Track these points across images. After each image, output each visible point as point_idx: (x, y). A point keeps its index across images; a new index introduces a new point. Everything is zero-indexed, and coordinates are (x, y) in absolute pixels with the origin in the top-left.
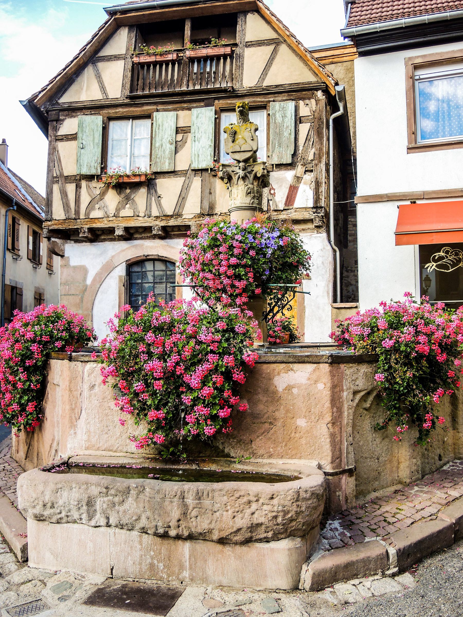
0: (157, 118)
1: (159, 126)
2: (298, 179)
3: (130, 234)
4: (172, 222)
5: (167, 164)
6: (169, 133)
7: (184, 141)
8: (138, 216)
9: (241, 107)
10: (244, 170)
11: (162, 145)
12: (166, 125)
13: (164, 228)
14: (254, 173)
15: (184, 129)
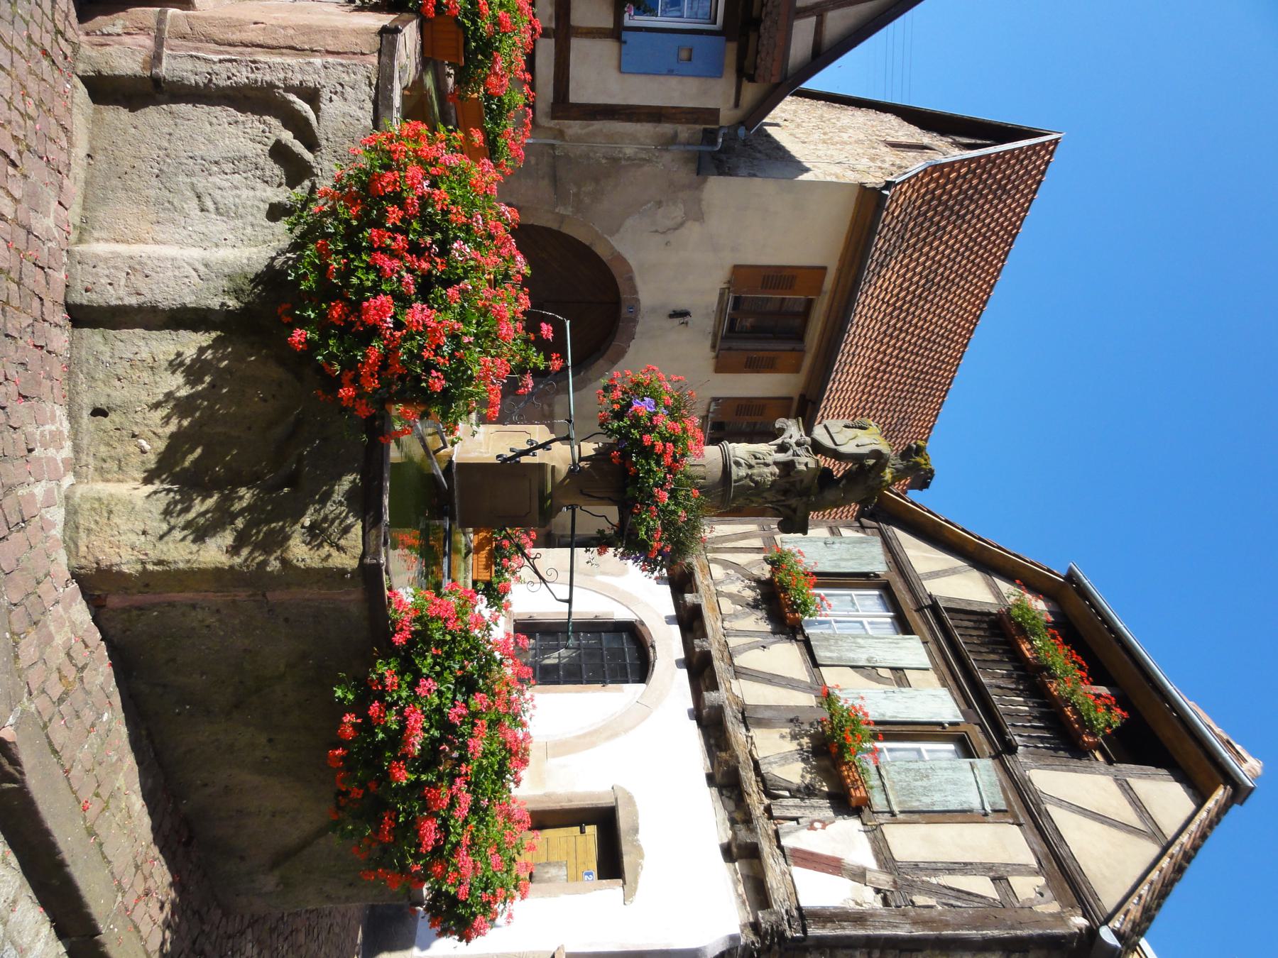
2: (859, 875)
3: (690, 621)
4: (718, 665)
7: (880, 680)
8: (723, 620)
13: (706, 658)
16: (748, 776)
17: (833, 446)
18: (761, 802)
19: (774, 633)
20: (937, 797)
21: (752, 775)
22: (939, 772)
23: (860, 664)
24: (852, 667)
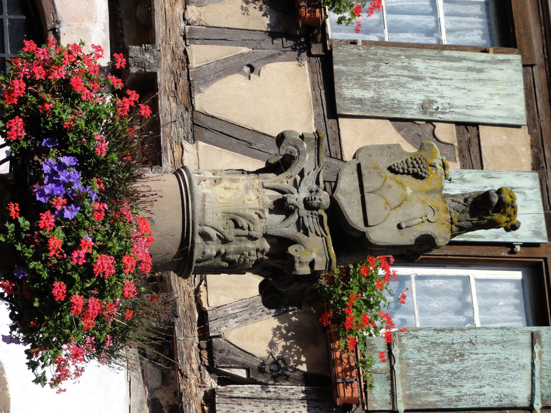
0: (504, 66)
1: (480, 71)
4: (168, 106)
5: (358, 93)
6: (457, 103)
9: (500, 199)
11: (419, 79)
12: (482, 92)
14: (300, 235)
15: (474, 149)
16: (188, 340)
17: (360, 226)
18: (201, 383)
19: (273, 34)
20: (469, 387)
21: (194, 338)
22: (481, 348)
23: (408, 115)
24: (392, 120)
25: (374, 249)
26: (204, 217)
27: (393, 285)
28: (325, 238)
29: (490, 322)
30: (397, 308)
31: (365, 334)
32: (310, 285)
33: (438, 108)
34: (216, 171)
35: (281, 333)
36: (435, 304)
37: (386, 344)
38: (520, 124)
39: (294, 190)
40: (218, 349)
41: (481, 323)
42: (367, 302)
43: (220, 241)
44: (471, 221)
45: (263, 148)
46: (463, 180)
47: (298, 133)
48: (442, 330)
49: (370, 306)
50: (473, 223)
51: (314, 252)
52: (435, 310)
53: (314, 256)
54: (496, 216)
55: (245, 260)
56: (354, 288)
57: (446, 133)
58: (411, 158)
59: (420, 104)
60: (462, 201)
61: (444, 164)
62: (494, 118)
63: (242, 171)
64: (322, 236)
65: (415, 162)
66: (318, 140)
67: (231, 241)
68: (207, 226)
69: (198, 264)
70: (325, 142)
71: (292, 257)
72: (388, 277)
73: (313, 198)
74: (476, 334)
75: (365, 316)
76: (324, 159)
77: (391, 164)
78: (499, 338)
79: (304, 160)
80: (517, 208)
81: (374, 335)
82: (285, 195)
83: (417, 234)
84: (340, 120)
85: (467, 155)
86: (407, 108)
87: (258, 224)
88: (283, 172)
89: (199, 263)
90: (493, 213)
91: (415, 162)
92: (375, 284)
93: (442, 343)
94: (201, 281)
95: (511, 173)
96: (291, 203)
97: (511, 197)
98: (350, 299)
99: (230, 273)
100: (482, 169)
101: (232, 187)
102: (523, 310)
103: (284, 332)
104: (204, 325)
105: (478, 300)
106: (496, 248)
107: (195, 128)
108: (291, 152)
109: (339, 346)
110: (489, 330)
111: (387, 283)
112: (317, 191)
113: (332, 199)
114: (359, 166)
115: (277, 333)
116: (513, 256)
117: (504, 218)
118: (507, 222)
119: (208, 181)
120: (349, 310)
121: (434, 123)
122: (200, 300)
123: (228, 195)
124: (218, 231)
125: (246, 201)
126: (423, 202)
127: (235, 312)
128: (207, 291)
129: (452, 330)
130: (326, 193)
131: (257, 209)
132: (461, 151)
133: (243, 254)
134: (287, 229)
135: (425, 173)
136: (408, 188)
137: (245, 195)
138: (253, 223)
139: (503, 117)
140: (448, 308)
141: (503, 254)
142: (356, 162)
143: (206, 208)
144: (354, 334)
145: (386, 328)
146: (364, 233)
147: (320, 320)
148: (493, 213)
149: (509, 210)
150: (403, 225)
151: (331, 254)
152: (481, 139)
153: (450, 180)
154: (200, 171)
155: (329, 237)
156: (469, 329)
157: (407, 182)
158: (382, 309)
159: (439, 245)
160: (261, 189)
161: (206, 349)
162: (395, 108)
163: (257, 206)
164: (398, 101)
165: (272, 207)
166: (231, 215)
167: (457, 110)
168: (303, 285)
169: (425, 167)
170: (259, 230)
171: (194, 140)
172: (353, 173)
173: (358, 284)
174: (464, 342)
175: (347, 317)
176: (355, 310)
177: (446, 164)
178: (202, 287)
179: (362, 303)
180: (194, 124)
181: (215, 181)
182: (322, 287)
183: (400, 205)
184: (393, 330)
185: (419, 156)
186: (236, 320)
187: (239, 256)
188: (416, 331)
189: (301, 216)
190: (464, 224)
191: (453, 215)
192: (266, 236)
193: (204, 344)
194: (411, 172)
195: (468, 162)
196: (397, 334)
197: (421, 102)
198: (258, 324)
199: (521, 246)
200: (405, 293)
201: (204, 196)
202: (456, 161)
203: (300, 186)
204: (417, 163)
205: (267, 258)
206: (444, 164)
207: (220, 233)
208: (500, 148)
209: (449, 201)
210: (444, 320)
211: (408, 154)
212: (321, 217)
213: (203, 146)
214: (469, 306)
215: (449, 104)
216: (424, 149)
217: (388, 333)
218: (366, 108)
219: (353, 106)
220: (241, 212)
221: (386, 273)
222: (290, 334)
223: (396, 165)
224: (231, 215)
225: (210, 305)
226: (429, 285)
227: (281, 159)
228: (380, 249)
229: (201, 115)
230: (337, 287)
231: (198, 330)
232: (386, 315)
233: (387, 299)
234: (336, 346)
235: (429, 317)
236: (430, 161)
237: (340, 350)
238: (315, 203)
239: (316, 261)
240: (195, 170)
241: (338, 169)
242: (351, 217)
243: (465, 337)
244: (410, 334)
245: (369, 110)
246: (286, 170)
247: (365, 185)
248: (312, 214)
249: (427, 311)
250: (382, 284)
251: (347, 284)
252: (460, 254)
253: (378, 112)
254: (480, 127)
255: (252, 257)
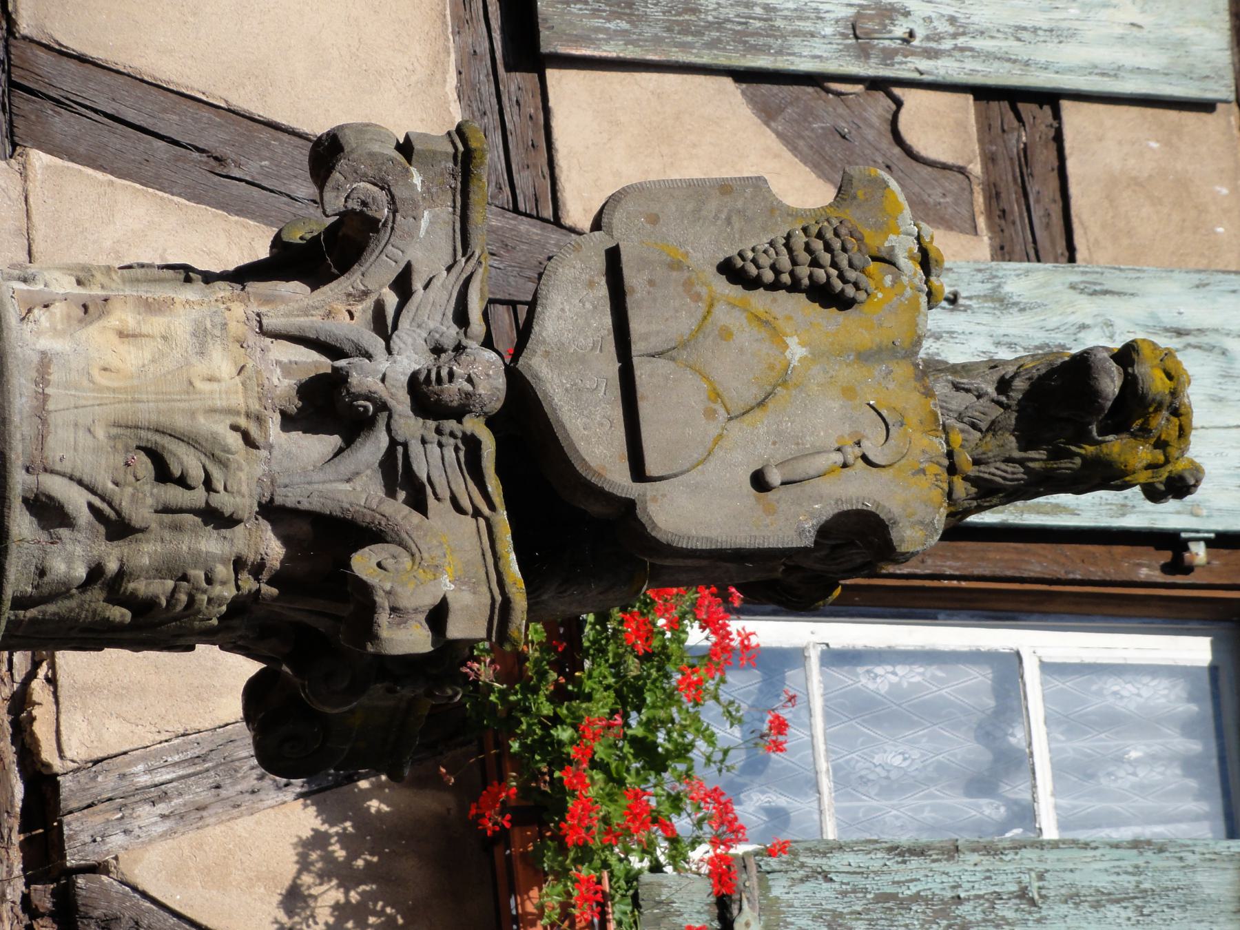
9: (1130, 384)
10: (425, 397)
14: (397, 510)
15: (1043, 188)
24: (742, 76)
25: (668, 562)
26: (42, 438)
27: (740, 684)
28: (487, 520)
29: (1094, 821)
30: (755, 767)
31: (637, 862)
32: (429, 694)
33: (912, 34)
34: (87, 269)
35: (329, 858)
36: (894, 755)
37: (712, 899)
38: (1210, 95)
39: (375, 343)
40: (97, 913)
41: (1062, 826)
42: (644, 748)
43: (102, 529)
44: (1021, 462)
45: (267, 175)
46: (1001, 300)
47: (389, 135)
48: (919, 851)
49: (654, 760)
50: (1028, 471)
51: (444, 573)
52: (893, 775)
53: (446, 585)
54: (1115, 446)
55: (191, 600)
56: (597, 696)
57: (941, 128)
58: (805, 230)
59: (846, 19)
60: (991, 390)
61: (924, 252)
62: (1116, 72)
63: (186, 273)
64: (477, 513)
65: (818, 245)
66: (466, 161)
67: (142, 530)
68: (52, 472)
69: (21, 613)
70: (496, 166)
71: (364, 590)
72: (722, 655)
73: (444, 373)
74: (1041, 867)
75: (637, 796)
76: (487, 219)
77: (733, 252)
78: (1128, 882)
79: (411, 234)
80: (1189, 414)
81: (669, 869)
82: (342, 363)
83: (824, 510)
84: (552, 75)
85: (1016, 209)
86: (797, 33)
87: (240, 469)
88: (334, 277)
89: (25, 608)
90: (1102, 432)
91: (818, 245)
92: (674, 682)
93: (916, 898)
94: (36, 665)
95: (1176, 275)
96: (364, 390)
97: (1170, 377)
98: (581, 737)
99: (136, 645)
100: (1072, 259)
101: (145, 329)
102: (1215, 778)
103: (340, 854)
104: (46, 825)
105: (1050, 739)
106: (1119, 550)
107: (16, 101)
108: (364, 204)
109: (541, 908)
110: (1090, 853)
111: (717, 676)
112: (459, 349)
113: (514, 377)
114: (613, 257)
115: (314, 856)
116: (1179, 579)
117: (1144, 453)
118: (1151, 466)
119: (58, 309)
120: (579, 776)
121: (897, 91)
122: (32, 734)
123: (131, 358)
124: (92, 491)
125: (199, 385)
126: (849, 392)
127: (158, 779)
128: (57, 703)
129: (953, 851)
130: (494, 355)
131: (238, 413)
132: (993, 194)
133: (185, 578)
134: (348, 487)
135: (857, 286)
136: (793, 342)
137: (194, 360)
138: (224, 464)
139: (1149, 72)
140: (941, 769)
141: (1144, 573)
142: (602, 242)
143: (51, 406)
144: (597, 863)
145: (715, 843)
146: (629, 505)
147: (473, 812)
148: (1102, 432)
149: (1161, 422)
150: (775, 477)
151: (508, 581)
152: (1067, 151)
153: (953, 300)
154: (33, 269)
155: (502, 518)
156: (1018, 846)
157: (789, 318)
158: (699, 772)
159: (903, 548)
160: (253, 339)
161: (53, 915)
162: (756, 34)
163: (238, 400)
164: (767, 8)
165: (294, 405)
166: (143, 433)
167: (978, 43)
168: (406, 692)
169: (856, 262)
170: (244, 489)
171: (14, 145)
172: (591, 284)
173: (611, 680)
174: (999, 896)
175: (570, 803)
176: (598, 776)
177: (932, 255)
178: (39, 688)
179: (627, 749)
180: (13, 85)
181: (85, 307)
182: (478, 690)
183: (761, 404)
184: (739, 849)
185: (835, 223)
186: (162, 808)
187: (170, 584)
188: (824, 854)
189: (400, 439)
190: (995, 471)
191: (957, 439)
192: (271, 511)
193: (43, 897)
194: (806, 281)
195: (1019, 235)
196: (751, 863)
197: (851, 12)
198: (243, 825)
199: (1209, 543)
200: (785, 714)
201: (45, 361)
202: (975, 230)
203: (395, 327)
204: (828, 248)
205: (275, 591)
206: (924, 252)
207: (103, 499)
208: (1136, 183)
209: (941, 387)
210: (927, 815)
211: (793, 214)
212: (472, 445)
213: (48, 167)
214: (1017, 762)
215: (952, 20)
216: (855, 197)
217: (722, 858)
218: (649, 32)
219: (598, 22)
220: (181, 423)
221: (713, 639)
222: (360, 863)
223: (750, 255)
224: (143, 433)
225: (68, 754)
226: (871, 686)
227: (331, 230)
228: (689, 562)
229: (42, 54)
230: (535, 690)
231: (23, 846)
232: (715, 794)
233: (719, 733)
234: (530, 908)
235: (868, 802)
236: (874, 242)
237: (545, 921)
238: (452, 392)
239: (454, 605)
240: (13, 266)
241: (542, 257)
242: (582, 446)
243: (1003, 878)
244: (803, 865)
245: (657, 40)
246: (344, 267)
247: (637, 326)
248: (439, 431)
249: (864, 781)
250: (700, 681)
251: (570, 678)
252: (987, 572)
253: (690, 46)
254: (1066, 105)
255: (217, 590)
